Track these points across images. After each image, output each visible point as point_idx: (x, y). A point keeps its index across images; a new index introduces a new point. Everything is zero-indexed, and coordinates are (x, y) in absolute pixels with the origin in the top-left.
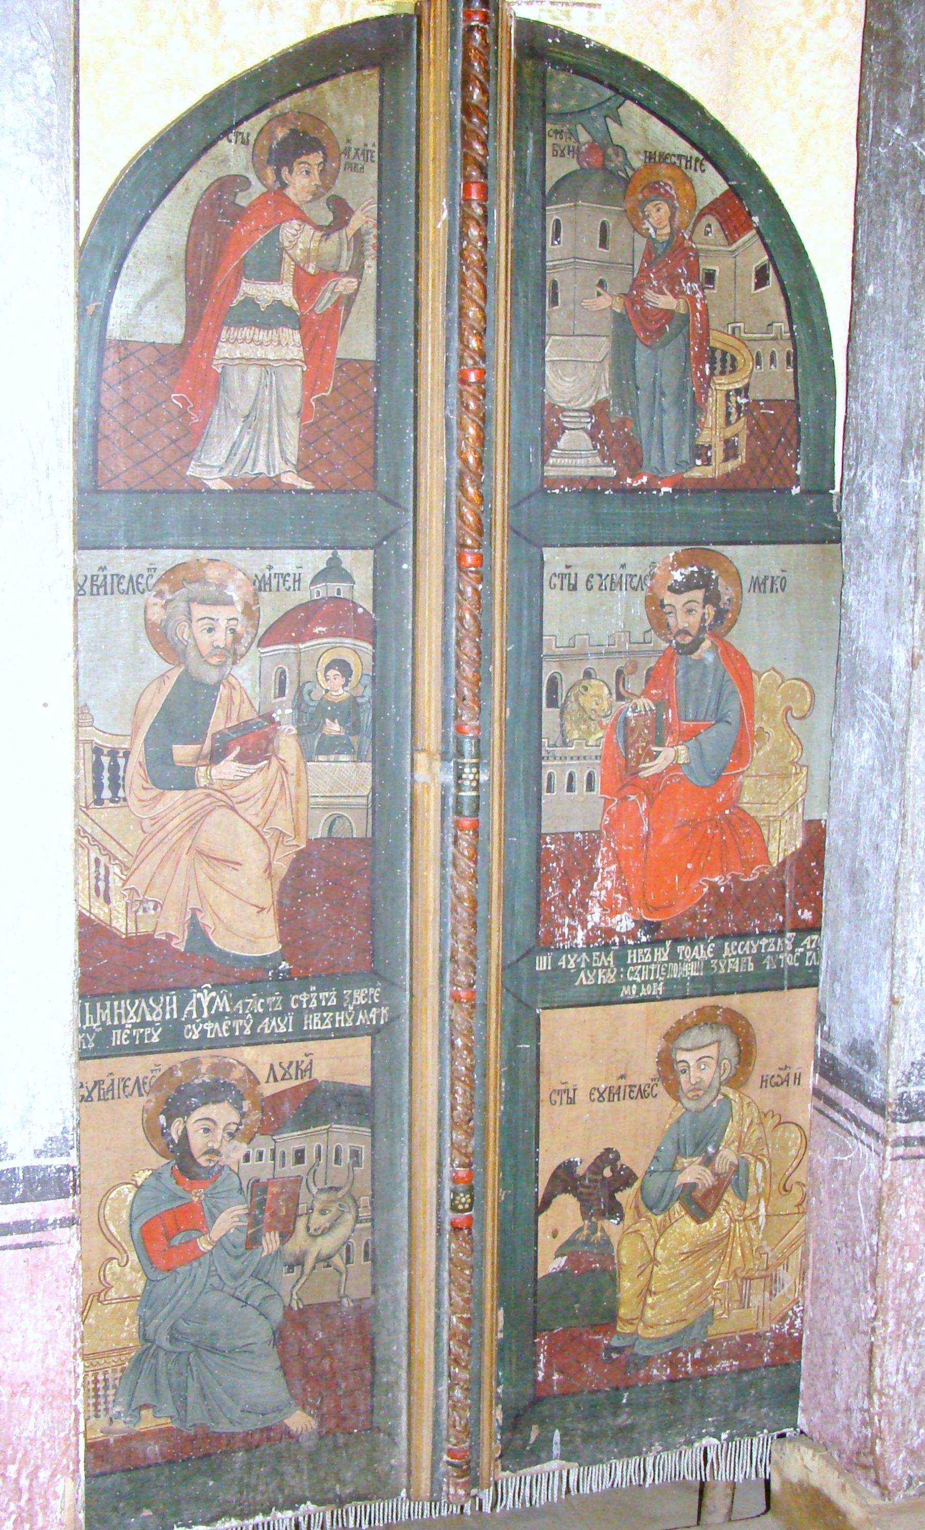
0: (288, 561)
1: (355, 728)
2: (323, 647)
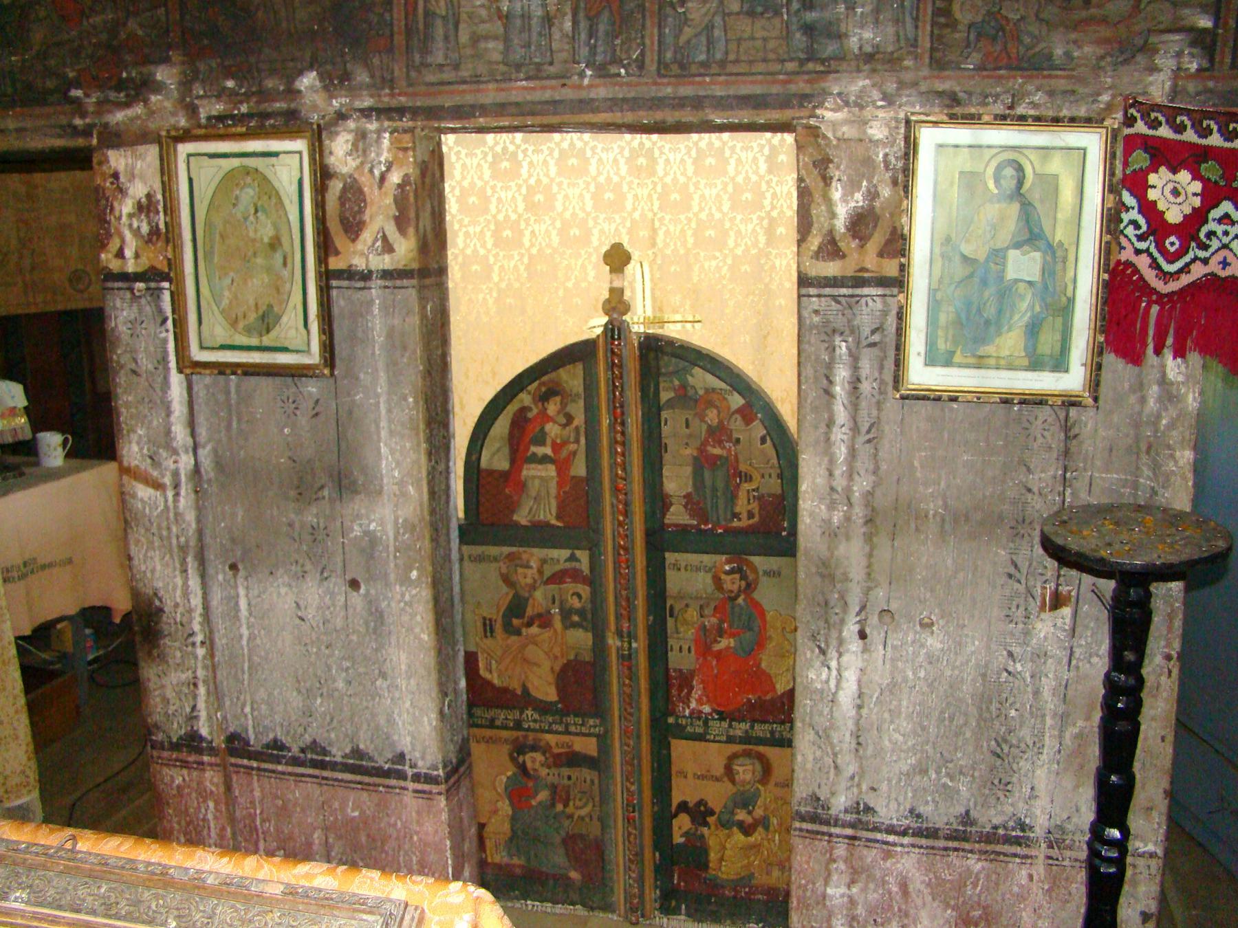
0: (555, 553)
1: (585, 619)
2: (570, 586)
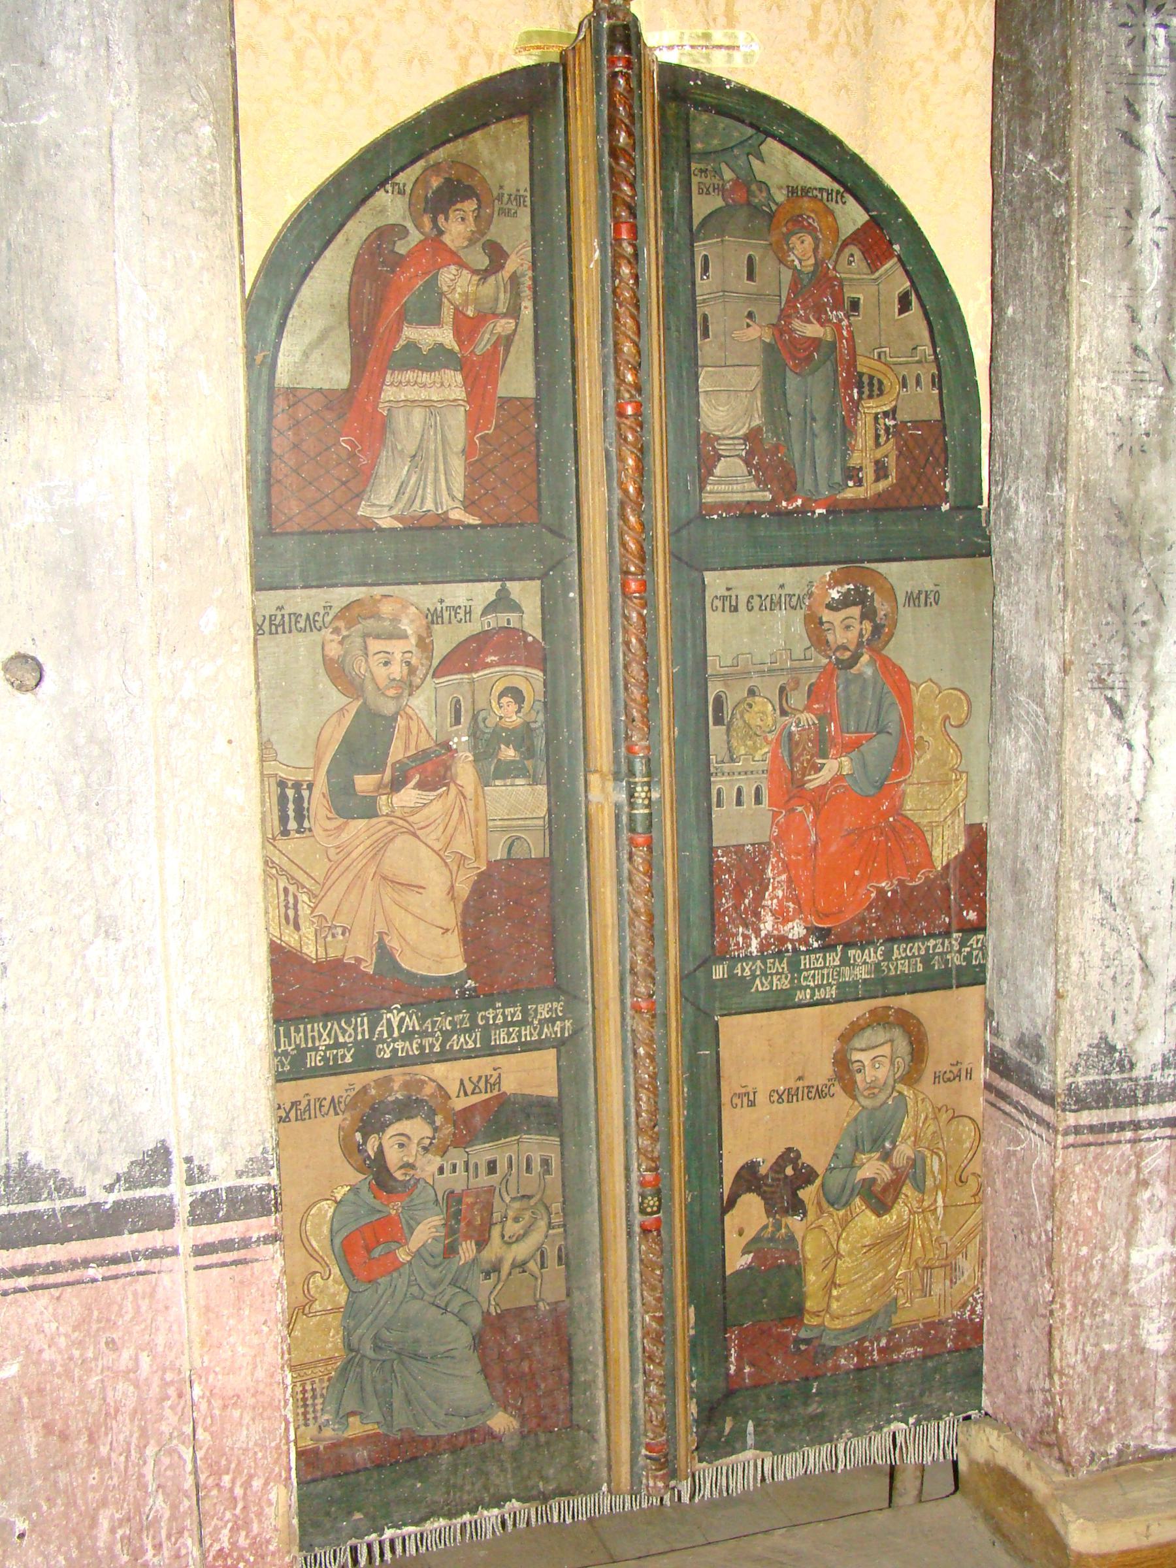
0: (459, 594)
2: (496, 675)
